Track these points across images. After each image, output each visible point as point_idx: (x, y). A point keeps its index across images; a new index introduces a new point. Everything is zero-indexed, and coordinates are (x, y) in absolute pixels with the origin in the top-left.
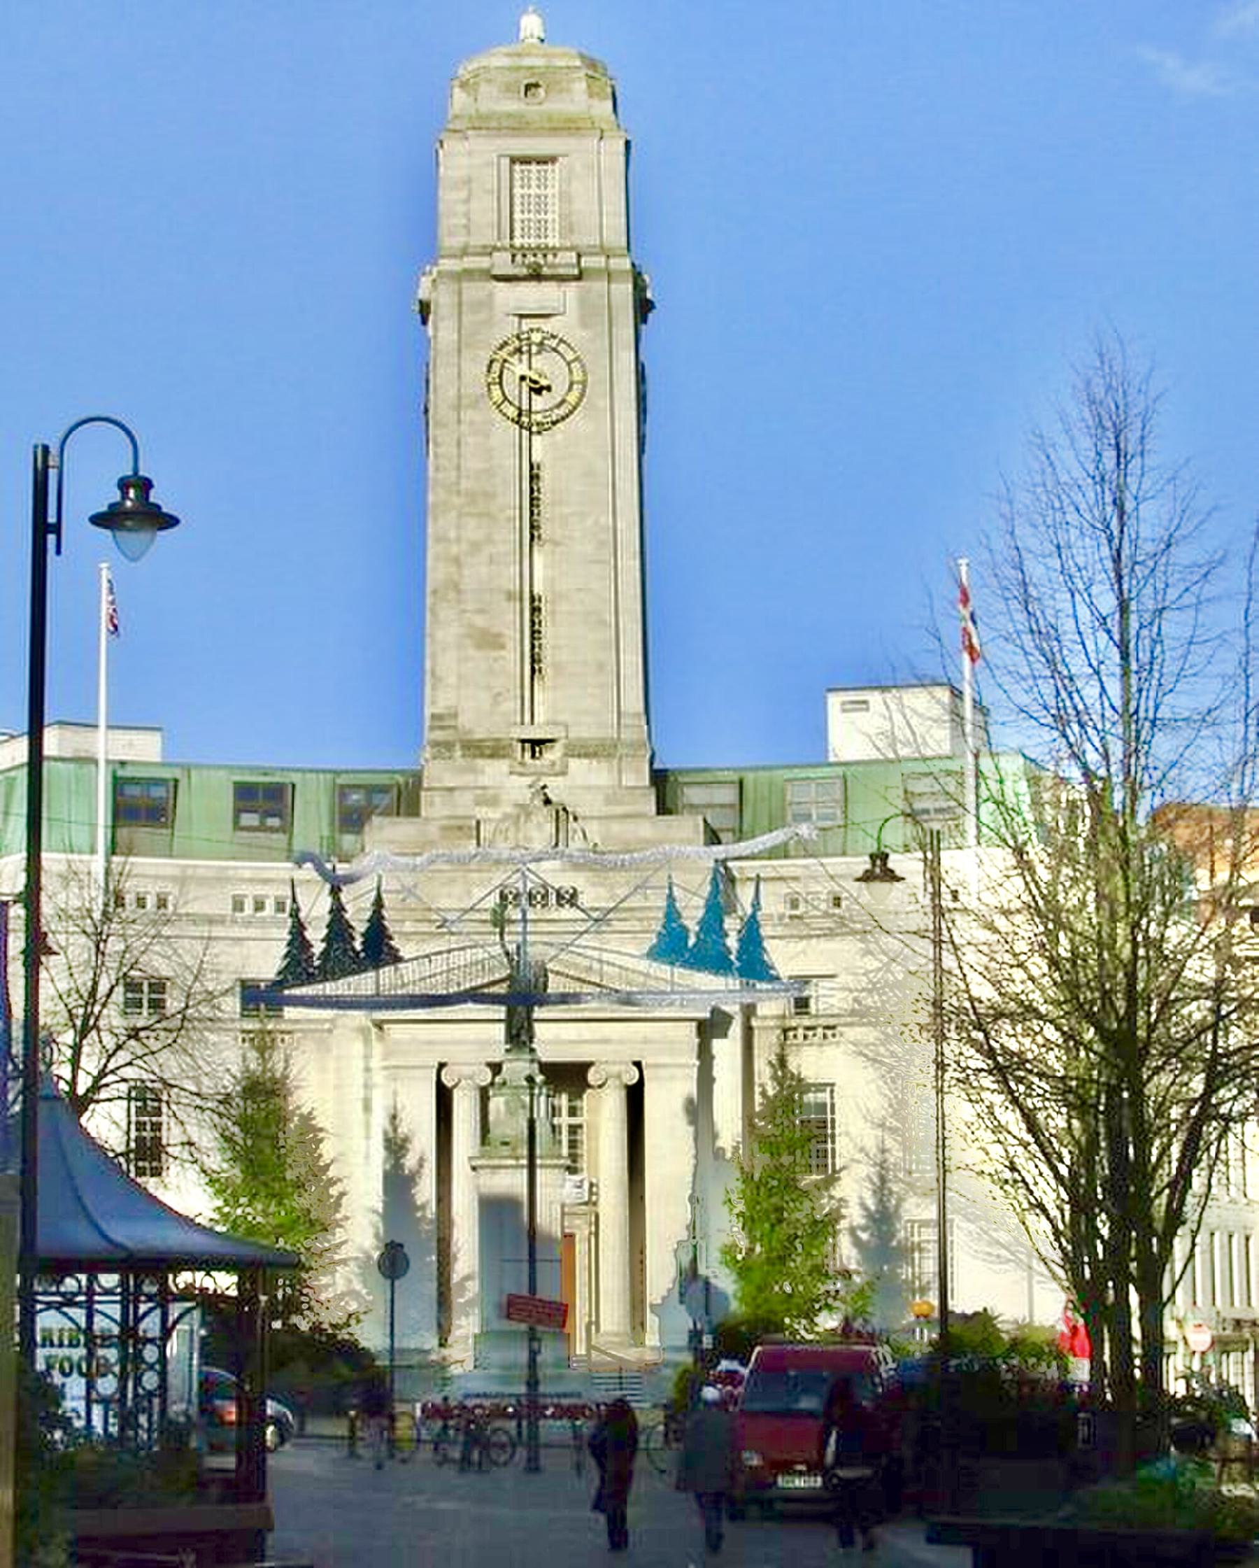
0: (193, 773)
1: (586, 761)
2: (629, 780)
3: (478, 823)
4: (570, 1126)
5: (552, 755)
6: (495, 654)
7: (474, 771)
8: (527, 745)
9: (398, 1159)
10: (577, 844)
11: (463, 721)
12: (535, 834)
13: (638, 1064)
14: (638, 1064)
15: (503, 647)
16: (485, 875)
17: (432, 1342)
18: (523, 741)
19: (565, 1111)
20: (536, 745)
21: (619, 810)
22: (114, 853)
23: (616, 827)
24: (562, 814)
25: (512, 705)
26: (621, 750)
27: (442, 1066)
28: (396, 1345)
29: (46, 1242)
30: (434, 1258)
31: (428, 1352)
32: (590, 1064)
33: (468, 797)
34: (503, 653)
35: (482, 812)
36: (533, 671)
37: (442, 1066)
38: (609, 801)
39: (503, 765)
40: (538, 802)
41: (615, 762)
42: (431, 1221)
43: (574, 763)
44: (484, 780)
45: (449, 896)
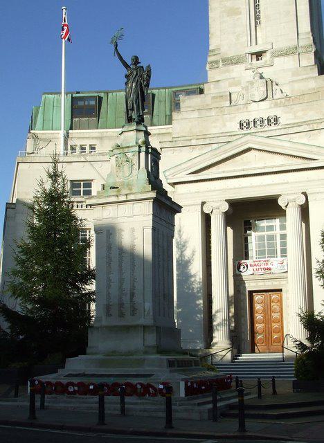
0: (110, 95)
1: (282, 58)
2: (304, 63)
3: (230, 94)
4: (281, 235)
5: (266, 58)
6: (238, 16)
7: (228, 71)
8: (254, 56)
9: (182, 252)
10: (278, 95)
11: (223, 50)
12: (255, 93)
13: (305, 194)
14: (305, 194)
15: (240, 13)
16: (233, 115)
17: (200, 345)
18: (252, 54)
19: (278, 228)
20: (259, 55)
21: (300, 78)
22: (71, 129)
23: (296, 86)
24: (269, 84)
25: (246, 38)
26: (300, 50)
27: (203, 203)
28: (148, 321)
29: (161, 426)
30: (201, 301)
31: (197, 351)
32: (280, 195)
33: (227, 83)
34: (240, 16)
35: (232, 90)
36: (256, 23)
37: (203, 203)
38: (293, 75)
39: (242, 67)
40: (257, 77)
41: (297, 56)
42: (200, 282)
43: (276, 60)
44: (234, 75)
45: (215, 127)
